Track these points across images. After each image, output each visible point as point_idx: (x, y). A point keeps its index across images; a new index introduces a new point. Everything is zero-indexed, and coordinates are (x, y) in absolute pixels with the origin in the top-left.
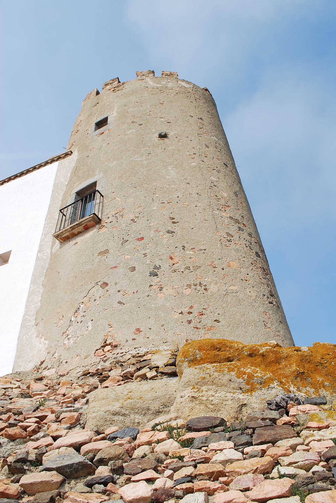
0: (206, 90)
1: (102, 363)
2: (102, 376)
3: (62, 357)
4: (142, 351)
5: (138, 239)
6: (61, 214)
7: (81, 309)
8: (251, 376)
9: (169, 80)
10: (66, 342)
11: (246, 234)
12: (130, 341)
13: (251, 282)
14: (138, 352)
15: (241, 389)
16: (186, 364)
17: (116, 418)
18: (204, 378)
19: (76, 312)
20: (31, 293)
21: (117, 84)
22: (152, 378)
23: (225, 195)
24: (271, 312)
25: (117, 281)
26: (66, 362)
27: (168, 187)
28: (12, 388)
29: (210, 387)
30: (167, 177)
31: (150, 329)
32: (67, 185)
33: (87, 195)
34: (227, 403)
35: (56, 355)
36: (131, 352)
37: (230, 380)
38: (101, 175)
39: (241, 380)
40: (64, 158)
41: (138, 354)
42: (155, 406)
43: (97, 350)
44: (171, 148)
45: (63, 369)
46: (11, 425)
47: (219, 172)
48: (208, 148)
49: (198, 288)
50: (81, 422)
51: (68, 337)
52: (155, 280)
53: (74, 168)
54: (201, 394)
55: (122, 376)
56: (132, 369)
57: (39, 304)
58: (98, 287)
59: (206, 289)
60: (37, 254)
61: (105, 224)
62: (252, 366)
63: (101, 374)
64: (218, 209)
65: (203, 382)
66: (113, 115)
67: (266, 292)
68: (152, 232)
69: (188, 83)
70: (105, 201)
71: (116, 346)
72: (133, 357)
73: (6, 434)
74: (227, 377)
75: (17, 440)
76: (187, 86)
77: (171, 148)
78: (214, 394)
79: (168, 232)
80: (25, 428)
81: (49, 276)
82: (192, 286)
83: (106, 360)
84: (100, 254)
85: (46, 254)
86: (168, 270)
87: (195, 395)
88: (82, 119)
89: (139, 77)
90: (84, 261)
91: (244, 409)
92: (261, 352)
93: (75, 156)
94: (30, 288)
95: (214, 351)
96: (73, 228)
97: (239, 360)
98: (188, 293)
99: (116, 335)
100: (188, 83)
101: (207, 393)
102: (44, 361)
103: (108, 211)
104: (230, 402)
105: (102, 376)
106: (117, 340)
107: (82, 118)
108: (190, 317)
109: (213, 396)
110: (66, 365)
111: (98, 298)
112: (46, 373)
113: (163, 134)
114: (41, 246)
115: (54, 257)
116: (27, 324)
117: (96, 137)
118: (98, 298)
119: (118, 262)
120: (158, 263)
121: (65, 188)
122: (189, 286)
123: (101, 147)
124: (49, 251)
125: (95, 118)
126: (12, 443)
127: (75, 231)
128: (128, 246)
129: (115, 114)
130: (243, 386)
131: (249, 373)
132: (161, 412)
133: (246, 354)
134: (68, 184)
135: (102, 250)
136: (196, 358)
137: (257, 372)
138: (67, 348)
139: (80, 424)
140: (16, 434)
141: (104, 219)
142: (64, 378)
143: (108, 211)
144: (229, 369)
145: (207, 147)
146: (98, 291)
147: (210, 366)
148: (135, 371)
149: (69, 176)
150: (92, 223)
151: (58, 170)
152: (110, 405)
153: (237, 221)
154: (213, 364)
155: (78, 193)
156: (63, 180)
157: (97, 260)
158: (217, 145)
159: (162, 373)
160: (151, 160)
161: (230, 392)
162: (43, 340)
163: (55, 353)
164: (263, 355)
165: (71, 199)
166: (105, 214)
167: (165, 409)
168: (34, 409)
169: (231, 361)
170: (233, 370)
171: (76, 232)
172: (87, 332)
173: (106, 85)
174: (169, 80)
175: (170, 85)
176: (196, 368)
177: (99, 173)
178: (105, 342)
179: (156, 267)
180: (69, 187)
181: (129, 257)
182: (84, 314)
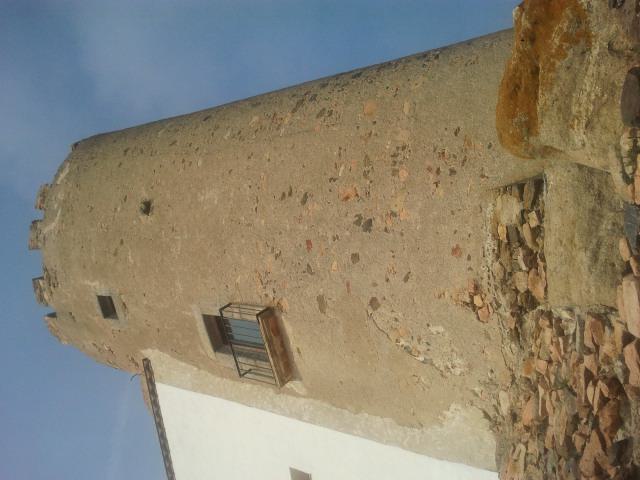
0: (76, 145)
1: (501, 310)
2: (525, 304)
3: (483, 378)
4: (490, 244)
5: (309, 248)
6: (248, 375)
7: (406, 344)
8: (566, 38)
9: (53, 198)
10: (458, 371)
11: (322, 91)
12: (472, 263)
13: (400, 83)
14: (491, 251)
15: (583, 53)
16: (532, 140)
17: (602, 257)
18: (559, 109)
19: (410, 353)
20: (368, 434)
21: (46, 281)
22: (540, 216)
23: (255, 119)
24: (452, 56)
25: (370, 282)
26: (492, 371)
27: (231, 202)
28: (527, 454)
29: (574, 100)
30: (216, 202)
31: (455, 232)
32: (199, 368)
33: (221, 332)
34: (603, 72)
35: (477, 389)
36: (490, 262)
37: (568, 68)
38: (194, 306)
39: (570, 53)
40: (151, 373)
41: (494, 250)
42: (589, 201)
43: (478, 318)
44: (168, 196)
45: (501, 375)
46: (596, 426)
47: (217, 127)
48: (176, 142)
49: (399, 158)
50: (603, 311)
51: (450, 366)
52: (378, 223)
53: (172, 356)
54: (584, 114)
55: (530, 269)
56: (520, 256)
57: (388, 420)
58: (376, 316)
59: (404, 148)
60: (305, 421)
61: (276, 302)
62: (550, 37)
63: (521, 308)
64: (278, 129)
65: (565, 113)
66: (98, 287)
67: (419, 62)
68: (301, 227)
69: (61, 169)
70: (239, 300)
71: (477, 287)
72: (498, 257)
73: (611, 432)
74: (563, 74)
75: (622, 415)
76: (67, 171)
77: (168, 196)
78: (585, 93)
79: (304, 202)
80: (604, 401)
81: (346, 401)
82: (397, 167)
83: (497, 303)
84: (322, 310)
85: (307, 407)
86: (363, 204)
87: (584, 121)
88: (90, 343)
89: (40, 244)
90: (329, 337)
91: (616, 47)
92: (529, 25)
93: (152, 354)
94: (358, 435)
95: (519, 94)
96: (274, 353)
97: (538, 57)
98: (406, 174)
99: (458, 287)
100: (61, 169)
101: (582, 104)
102: (484, 412)
103: (255, 296)
104: (603, 67)
105: (525, 304)
106: (466, 286)
107: (88, 344)
108: (445, 171)
109: (589, 95)
110: (497, 373)
111: (393, 315)
112: (505, 409)
113: (143, 206)
114: (291, 415)
115: (315, 392)
116: (418, 442)
117: (129, 317)
118: (393, 315)
119: (340, 281)
120: (351, 219)
121: (202, 372)
122: (395, 173)
123: (147, 307)
124: (302, 401)
125: (96, 318)
126: (627, 424)
127: (279, 350)
128: (318, 265)
129: (96, 283)
130: (578, 49)
131: (560, 40)
132: (600, 192)
133: (529, 47)
134: (197, 366)
135: (317, 307)
136: (525, 122)
137: (561, 29)
138: (467, 369)
139: (606, 314)
140: (611, 416)
141: (267, 302)
142: (518, 375)
143: (255, 296)
144: (549, 71)
145: (174, 143)
146: (383, 315)
147: (541, 101)
148: (523, 249)
149: (183, 364)
150: (271, 320)
151: (171, 384)
152: (579, 269)
153: (301, 103)
154: (540, 95)
155: (217, 348)
156: (189, 375)
157: (331, 316)
158: (172, 129)
159: (535, 202)
160: (185, 227)
161: (586, 70)
162: (448, 414)
163: (473, 391)
164: (535, 24)
165: (226, 361)
166: (259, 301)
167: (596, 186)
168: (571, 396)
169: (538, 69)
170: (554, 64)
171: (282, 350)
172: (447, 334)
173: (41, 299)
174: (53, 198)
175: (61, 196)
176: (542, 122)
177: (190, 310)
178: (467, 304)
179: (358, 223)
180: (201, 365)
181: (335, 263)
182: (416, 339)
